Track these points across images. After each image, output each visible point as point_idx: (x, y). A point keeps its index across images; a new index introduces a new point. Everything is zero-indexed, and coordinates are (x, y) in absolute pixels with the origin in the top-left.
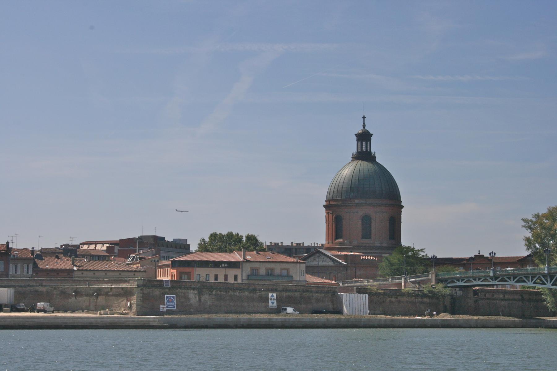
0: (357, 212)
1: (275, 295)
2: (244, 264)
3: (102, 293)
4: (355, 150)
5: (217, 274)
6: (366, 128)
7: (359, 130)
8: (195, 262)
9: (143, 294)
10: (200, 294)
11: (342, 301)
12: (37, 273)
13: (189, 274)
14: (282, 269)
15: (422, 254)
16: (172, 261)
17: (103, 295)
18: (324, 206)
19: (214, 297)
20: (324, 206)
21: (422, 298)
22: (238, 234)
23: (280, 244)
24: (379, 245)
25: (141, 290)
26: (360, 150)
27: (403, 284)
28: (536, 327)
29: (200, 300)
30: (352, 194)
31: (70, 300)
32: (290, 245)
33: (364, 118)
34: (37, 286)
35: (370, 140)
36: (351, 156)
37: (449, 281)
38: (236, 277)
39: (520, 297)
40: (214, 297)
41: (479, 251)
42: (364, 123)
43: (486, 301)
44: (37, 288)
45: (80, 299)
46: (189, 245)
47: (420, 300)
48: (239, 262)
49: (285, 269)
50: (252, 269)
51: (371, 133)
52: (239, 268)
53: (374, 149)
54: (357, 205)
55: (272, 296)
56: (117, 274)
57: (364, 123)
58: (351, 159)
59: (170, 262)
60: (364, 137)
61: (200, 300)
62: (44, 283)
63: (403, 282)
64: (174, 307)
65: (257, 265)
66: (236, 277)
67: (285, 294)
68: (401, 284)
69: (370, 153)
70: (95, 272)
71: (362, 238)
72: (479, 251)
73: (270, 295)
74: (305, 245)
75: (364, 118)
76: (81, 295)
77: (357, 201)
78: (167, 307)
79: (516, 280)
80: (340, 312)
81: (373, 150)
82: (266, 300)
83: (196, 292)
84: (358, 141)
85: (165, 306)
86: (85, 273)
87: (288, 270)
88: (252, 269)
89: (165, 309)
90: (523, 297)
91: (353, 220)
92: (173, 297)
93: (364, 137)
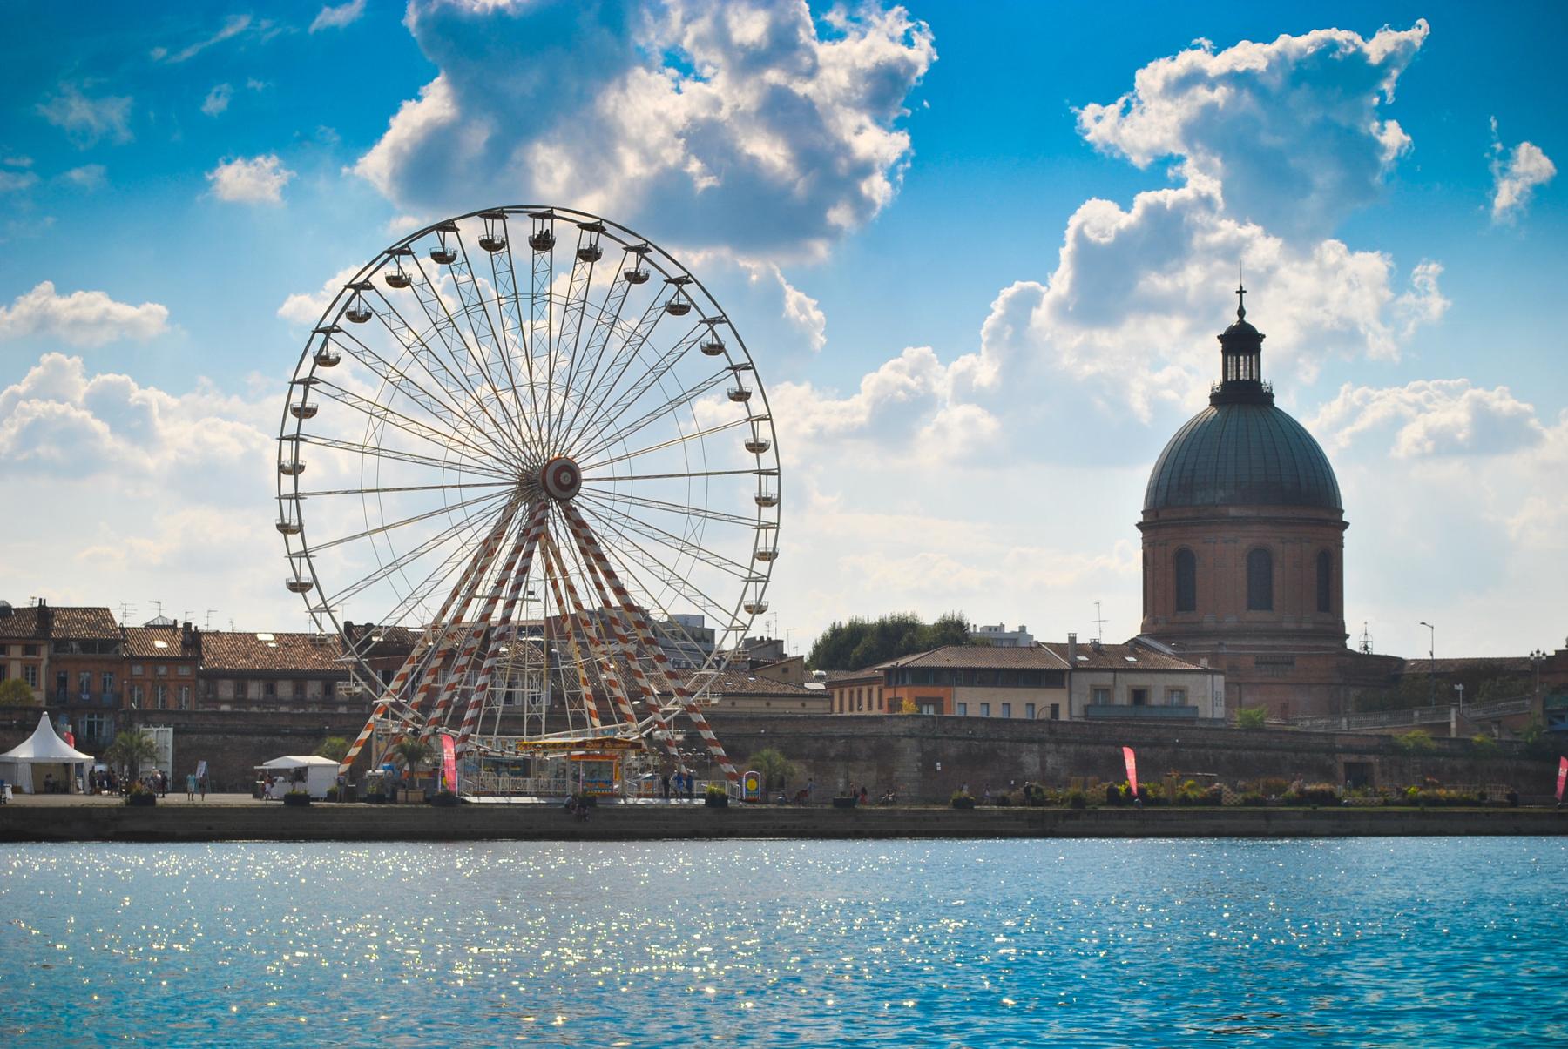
2: (1076, 676)
8: (953, 671)
13: (937, 702)
16: (886, 670)
20: (1139, 526)
24: (1292, 626)
27: (1453, 725)
30: (1221, 493)
42: (1241, 307)
48: (1062, 672)
50: (1097, 690)
53: (1269, 374)
54: (1236, 521)
55: (161, 737)
57: (1241, 307)
59: (882, 674)
60: (1242, 342)
63: (1453, 719)
68: (1448, 724)
71: (1250, 607)
74: (1008, 630)
75: (1241, 292)
76: (516, 763)
77: (1233, 512)
81: (1265, 378)
84: (1225, 352)
87: (1182, 691)
91: (1224, 558)
93: (1242, 342)
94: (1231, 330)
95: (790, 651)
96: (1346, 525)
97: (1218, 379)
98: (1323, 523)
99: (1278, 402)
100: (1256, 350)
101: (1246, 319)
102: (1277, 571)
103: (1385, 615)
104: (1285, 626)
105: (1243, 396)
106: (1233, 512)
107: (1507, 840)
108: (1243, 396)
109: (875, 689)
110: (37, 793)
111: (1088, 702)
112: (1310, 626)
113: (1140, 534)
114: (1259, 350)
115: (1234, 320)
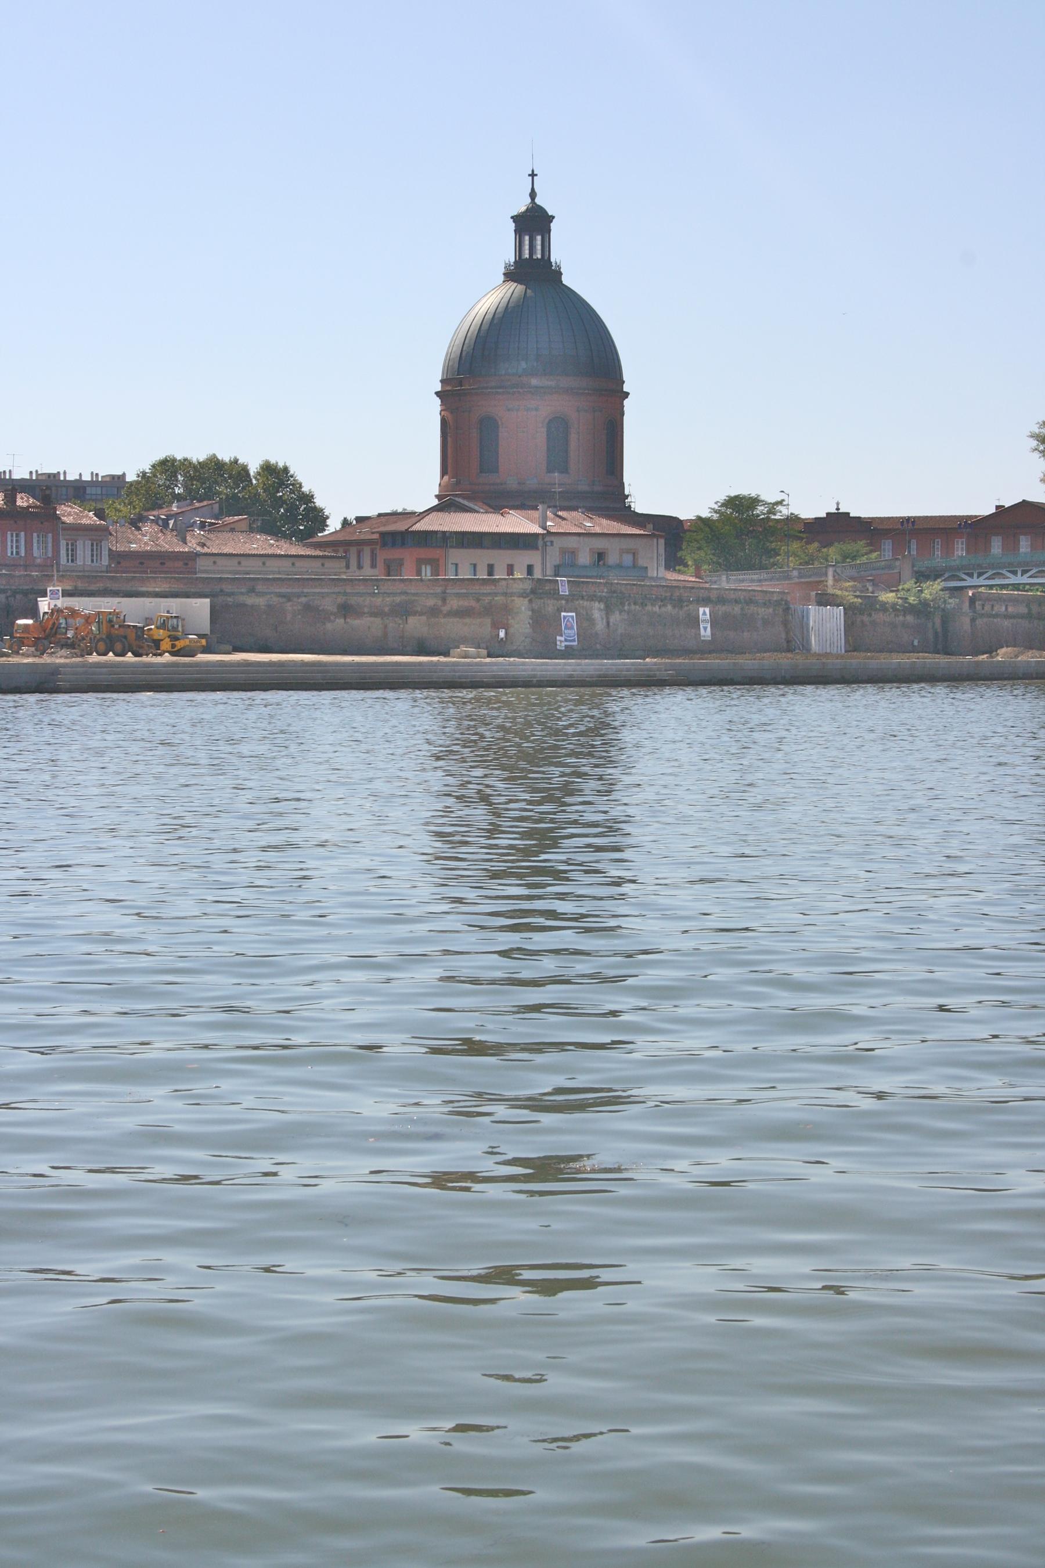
0: (536, 410)
1: (707, 610)
3: (366, 610)
4: (509, 255)
5: (491, 562)
6: (538, 201)
7: (522, 205)
9: (533, 610)
10: (608, 610)
11: (808, 624)
12: (119, 563)
14: (622, 552)
15: (784, 512)
17: (421, 614)
18: (437, 393)
19: (626, 617)
20: (437, 393)
21: (904, 616)
22: (236, 461)
23: (62, 478)
25: (530, 601)
28: (955, 679)
29: (608, 623)
30: (524, 365)
31: (329, 626)
32: (28, 477)
34: (242, 593)
36: (503, 270)
37: (946, 575)
38: (530, 569)
39: (1026, 611)
40: (626, 617)
41: (838, 504)
42: (533, 189)
43: (985, 620)
44: (242, 599)
45: (356, 622)
46: (828, 514)
47: (901, 618)
49: (628, 551)
50: (563, 551)
52: (537, 549)
56: (258, 562)
57: (533, 189)
58: (502, 278)
60: (533, 223)
61: (608, 623)
62: (260, 588)
64: (574, 641)
65: (572, 543)
66: (530, 569)
67: (722, 609)
69: (546, 261)
70: (242, 559)
72: (838, 504)
73: (701, 610)
75: (533, 175)
77: (534, 382)
78: (566, 640)
80: (806, 647)
82: (695, 622)
83: (602, 606)
84: (519, 232)
85: (563, 639)
86: (221, 561)
88: (563, 551)
89: (563, 644)
90: (1030, 610)
92: (572, 617)
93: (533, 223)
96: (627, 395)
97: (511, 258)
99: (566, 280)
100: (546, 232)
101: (538, 201)
103: (670, 473)
107: (338, 692)
109: (367, 550)
111: (558, 562)
113: (438, 401)
114: (549, 231)
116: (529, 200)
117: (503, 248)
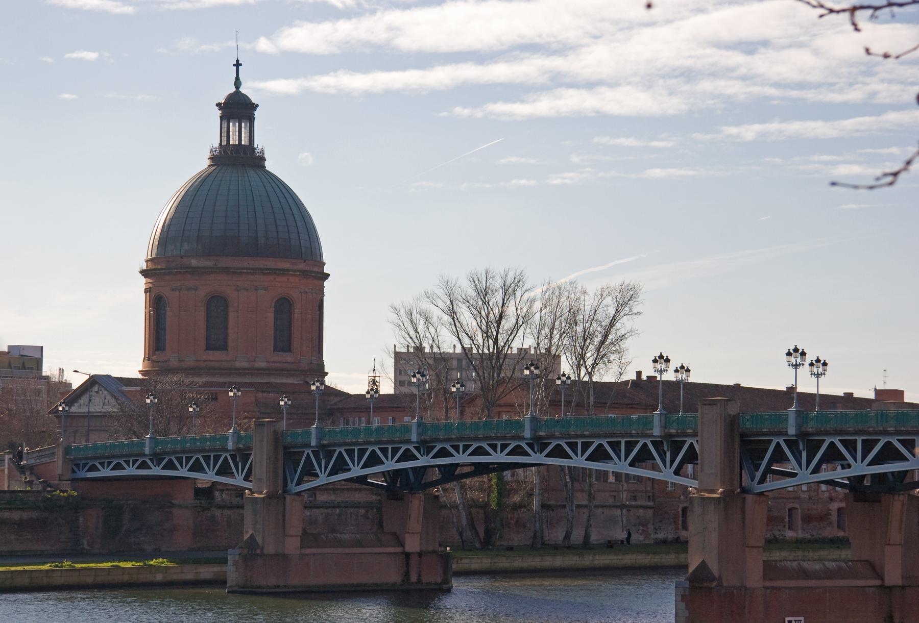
24: (246, 365)
26: (234, 141)
30: (186, 246)
33: (238, 65)
35: (251, 120)
36: (208, 155)
42: (237, 78)
51: (254, 100)
57: (237, 78)
60: (238, 109)
75: (238, 65)
79: (86, 468)
84: (222, 118)
93: (238, 109)
94: (230, 97)
95: (326, 378)
96: (327, 276)
98: (305, 274)
99: (269, 166)
101: (243, 90)
102: (232, 315)
104: (238, 364)
105: (238, 161)
106: (194, 262)
108: (238, 161)
110: (913, 470)
112: (263, 365)
115: (233, 89)
116: (233, 89)
117: (204, 136)
